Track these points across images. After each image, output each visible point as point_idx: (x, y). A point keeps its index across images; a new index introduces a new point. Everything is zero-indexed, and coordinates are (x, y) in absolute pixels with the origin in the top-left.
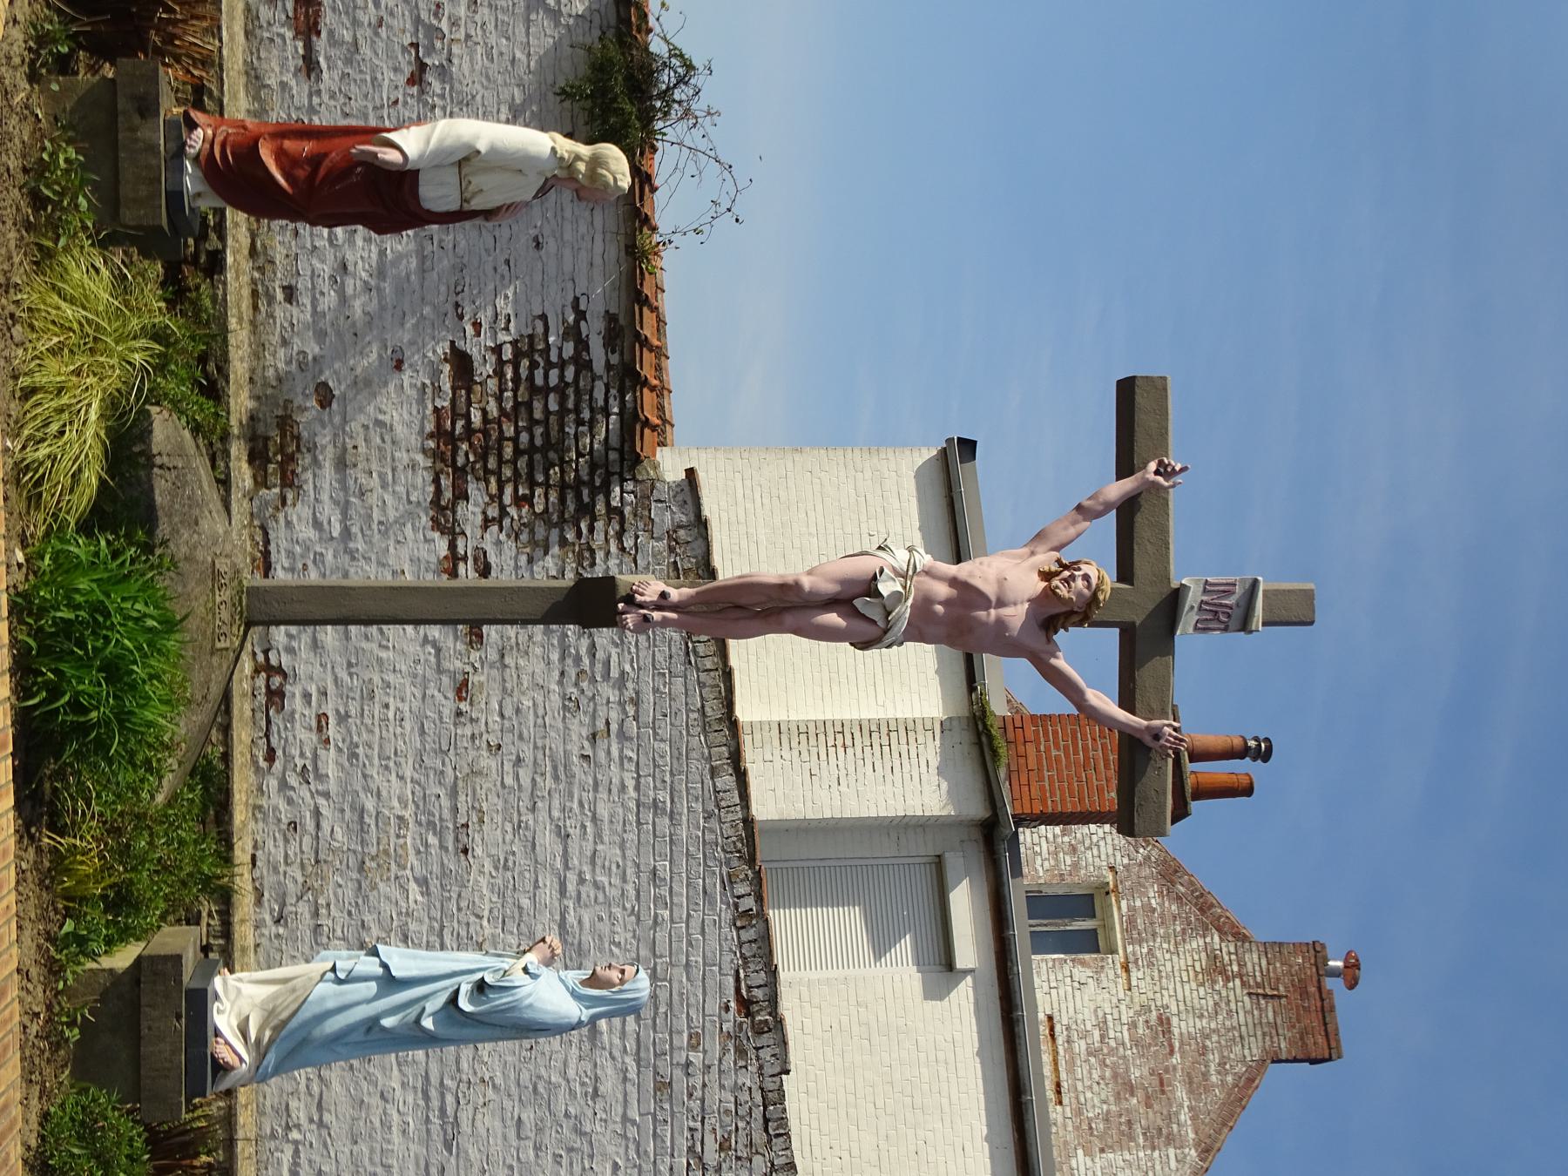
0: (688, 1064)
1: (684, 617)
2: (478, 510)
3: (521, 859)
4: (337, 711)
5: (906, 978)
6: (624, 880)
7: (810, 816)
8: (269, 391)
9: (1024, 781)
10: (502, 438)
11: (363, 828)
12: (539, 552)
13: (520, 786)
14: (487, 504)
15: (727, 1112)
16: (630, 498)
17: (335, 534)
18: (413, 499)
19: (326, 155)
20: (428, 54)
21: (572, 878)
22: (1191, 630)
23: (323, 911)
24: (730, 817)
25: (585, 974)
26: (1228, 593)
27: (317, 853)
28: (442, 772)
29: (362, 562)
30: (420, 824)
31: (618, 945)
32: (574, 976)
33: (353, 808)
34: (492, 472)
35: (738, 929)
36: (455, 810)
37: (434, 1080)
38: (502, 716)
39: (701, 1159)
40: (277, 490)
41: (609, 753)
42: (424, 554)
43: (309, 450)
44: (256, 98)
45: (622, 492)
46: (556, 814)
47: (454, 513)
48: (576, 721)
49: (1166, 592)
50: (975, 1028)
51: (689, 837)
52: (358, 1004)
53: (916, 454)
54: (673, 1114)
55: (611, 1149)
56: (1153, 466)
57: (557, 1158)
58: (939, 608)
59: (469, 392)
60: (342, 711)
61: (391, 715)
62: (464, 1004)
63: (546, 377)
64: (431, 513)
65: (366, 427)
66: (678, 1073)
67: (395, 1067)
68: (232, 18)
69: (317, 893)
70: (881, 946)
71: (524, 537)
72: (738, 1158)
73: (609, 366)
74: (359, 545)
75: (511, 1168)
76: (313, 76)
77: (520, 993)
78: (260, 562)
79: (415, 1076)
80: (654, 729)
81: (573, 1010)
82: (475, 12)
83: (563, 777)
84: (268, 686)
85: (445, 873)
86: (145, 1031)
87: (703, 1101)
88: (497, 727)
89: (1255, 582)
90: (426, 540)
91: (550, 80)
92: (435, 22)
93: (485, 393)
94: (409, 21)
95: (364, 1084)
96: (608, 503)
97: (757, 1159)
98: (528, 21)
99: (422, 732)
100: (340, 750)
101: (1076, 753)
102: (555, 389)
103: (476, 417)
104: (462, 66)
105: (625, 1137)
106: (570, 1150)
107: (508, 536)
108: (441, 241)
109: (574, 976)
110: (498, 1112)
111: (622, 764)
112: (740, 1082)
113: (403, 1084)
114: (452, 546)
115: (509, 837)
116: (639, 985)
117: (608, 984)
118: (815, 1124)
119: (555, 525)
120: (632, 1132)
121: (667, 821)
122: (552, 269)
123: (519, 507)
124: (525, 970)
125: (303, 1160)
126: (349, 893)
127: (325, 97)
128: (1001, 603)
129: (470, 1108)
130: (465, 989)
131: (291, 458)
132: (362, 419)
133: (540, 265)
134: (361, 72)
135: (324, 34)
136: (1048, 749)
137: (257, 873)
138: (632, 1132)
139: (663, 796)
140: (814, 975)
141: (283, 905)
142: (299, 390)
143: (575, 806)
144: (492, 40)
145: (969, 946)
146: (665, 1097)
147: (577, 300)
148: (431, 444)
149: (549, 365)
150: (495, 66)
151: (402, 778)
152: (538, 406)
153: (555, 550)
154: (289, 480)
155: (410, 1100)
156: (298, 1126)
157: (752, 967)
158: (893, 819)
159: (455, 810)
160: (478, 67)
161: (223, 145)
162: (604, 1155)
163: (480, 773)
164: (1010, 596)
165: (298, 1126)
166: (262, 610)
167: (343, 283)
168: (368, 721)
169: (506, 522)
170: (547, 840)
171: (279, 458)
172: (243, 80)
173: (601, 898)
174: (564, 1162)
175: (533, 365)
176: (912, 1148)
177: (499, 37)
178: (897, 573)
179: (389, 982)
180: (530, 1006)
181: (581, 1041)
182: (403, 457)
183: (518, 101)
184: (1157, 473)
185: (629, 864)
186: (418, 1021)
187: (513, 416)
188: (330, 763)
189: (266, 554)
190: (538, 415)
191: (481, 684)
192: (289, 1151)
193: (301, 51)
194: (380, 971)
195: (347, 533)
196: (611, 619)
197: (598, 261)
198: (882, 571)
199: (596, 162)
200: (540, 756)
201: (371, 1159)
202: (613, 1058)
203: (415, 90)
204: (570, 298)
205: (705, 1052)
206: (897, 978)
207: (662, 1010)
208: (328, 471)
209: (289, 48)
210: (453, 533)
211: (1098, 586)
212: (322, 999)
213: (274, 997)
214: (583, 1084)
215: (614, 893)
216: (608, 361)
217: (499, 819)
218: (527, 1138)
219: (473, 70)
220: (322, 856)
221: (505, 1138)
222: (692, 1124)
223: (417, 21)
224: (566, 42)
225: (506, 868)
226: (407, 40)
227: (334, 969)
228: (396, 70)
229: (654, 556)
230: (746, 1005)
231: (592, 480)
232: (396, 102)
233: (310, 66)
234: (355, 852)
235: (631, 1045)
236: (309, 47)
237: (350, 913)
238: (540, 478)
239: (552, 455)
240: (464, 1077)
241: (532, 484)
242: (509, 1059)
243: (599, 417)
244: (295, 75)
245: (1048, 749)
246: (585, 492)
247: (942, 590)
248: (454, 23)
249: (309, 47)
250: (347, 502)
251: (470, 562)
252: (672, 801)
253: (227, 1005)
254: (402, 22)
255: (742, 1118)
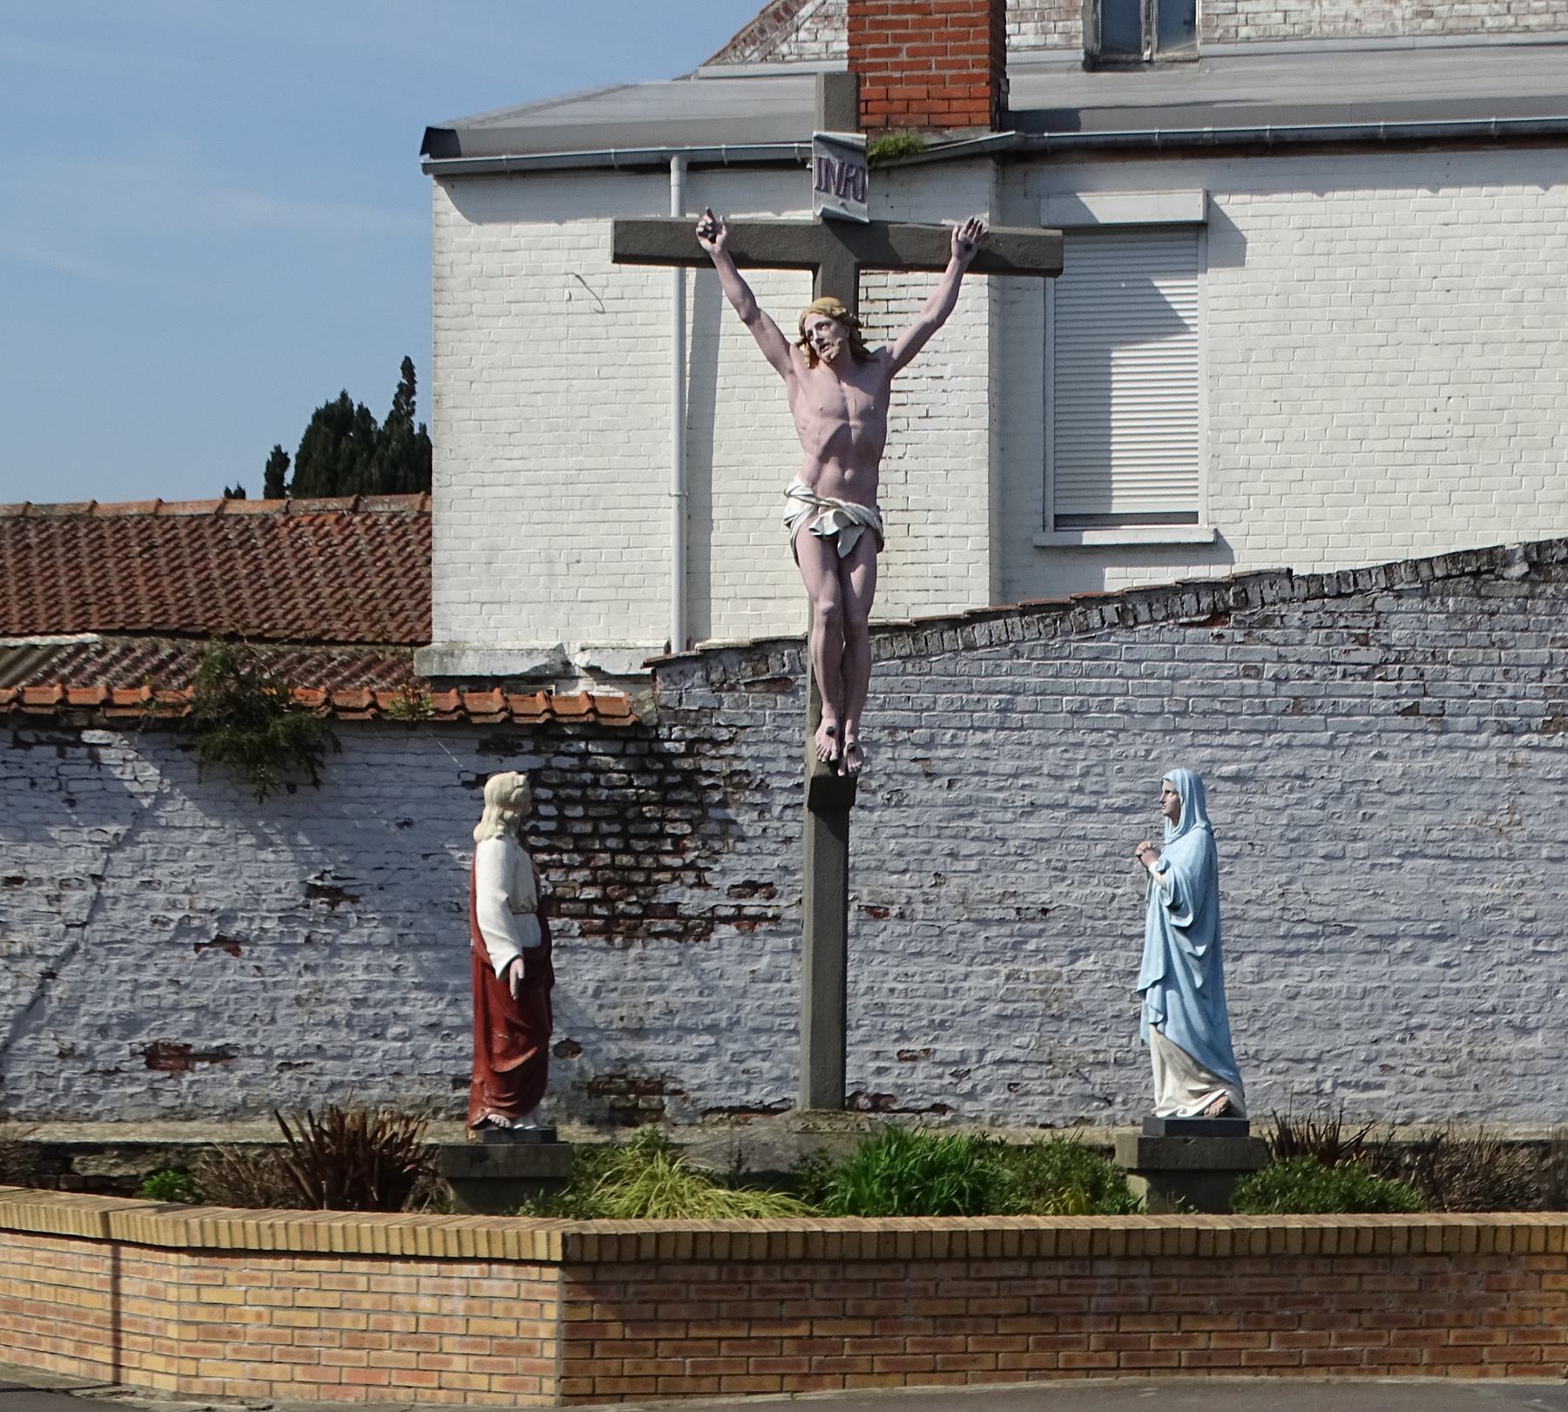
0: (1276, 678)
1: (850, 713)
2: (688, 893)
3: (1055, 854)
4: (896, 1040)
5: (1212, 290)
6: (1081, 744)
7: (985, 421)
8: (563, 1105)
9: (943, 106)
10: (612, 866)
11: (1018, 1016)
12: (733, 829)
13: (979, 854)
14: (682, 883)
15: (1328, 637)
16: (676, 732)
17: (712, 1040)
18: (676, 960)
19: (507, 1020)
20: (206, 933)
21: (1076, 800)
22: (865, 206)
23: (1101, 1057)
24: (1018, 630)
25: (1167, 821)
26: (829, 165)
27: (1041, 1063)
28: (962, 934)
29: (742, 1013)
30: (1015, 957)
31: (1148, 752)
32: (1169, 831)
33: (997, 1026)
34: (648, 877)
35: (1137, 623)
36: (1002, 921)
37: (1279, 944)
38: (905, 871)
39: (1375, 666)
40: (666, 1099)
41: (946, 759)
42: (735, 950)
43: (624, 1066)
44: (256, 1111)
45: (669, 740)
46: (1009, 816)
47: (691, 918)
48: (912, 793)
49: (827, 230)
50: (1286, 196)
51: (1038, 675)
52: (1183, 1005)
53: (444, 219)
54: (1326, 696)
55: (1360, 762)
56: (705, 243)
57: (1367, 818)
58: (848, 474)
59: (563, 899)
60: (896, 1036)
61: (901, 986)
62: (1187, 922)
63: (547, 818)
64: (691, 941)
65: (601, 1007)
66: (1285, 689)
67: (1263, 985)
68: (176, 1133)
69: (1082, 1063)
70: (1165, 323)
71: (717, 845)
72: (1377, 626)
73: (536, 752)
74: (723, 1017)
75: (1373, 866)
76: (232, 1053)
77: (1180, 876)
78: (740, 1117)
79: (1273, 965)
80: (922, 711)
81: (1197, 833)
82: (160, 883)
83: (970, 809)
84: (868, 1111)
85: (1066, 933)
86: (1196, 1166)
87: (1315, 664)
88: (916, 877)
89: (818, 138)
90: (720, 947)
91: (228, 806)
92: (172, 926)
93: (565, 884)
94: (172, 953)
95: (1279, 1016)
96: (682, 756)
97: (1379, 605)
98: (168, 827)
99: (920, 954)
100: (936, 1039)
101: (904, 24)
102: (560, 809)
103: (590, 893)
104: (220, 899)
105: (1348, 746)
106: (1358, 804)
107: (716, 861)
108: (404, 926)
109: (1169, 831)
110: (1316, 879)
111: (958, 746)
112: (1298, 623)
113: (1282, 977)
114: (726, 920)
115: (1031, 866)
116: (1179, 778)
117: (1177, 806)
118: (1404, 431)
119: (705, 812)
120: (1344, 739)
121: (1020, 698)
122: (433, 810)
123: (685, 850)
124: (1162, 872)
125: (1353, 1078)
126: (1084, 1030)
127: (254, 1041)
128: (844, 415)
129: (1310, 908)
130: (1175, 921)
131: (633, 1085)
132: (592, 1011)
133: (429, 823)
134: (227, 1003)
135: (188, 1041)
136: (900, 66)
137: (1060, 1123)
138: (1344, 739)
139: (994, 701)
140: (1204, 421)
141: (1093, 1097)
142: (562, 1074)
143: (1001, 795)
144: (190, 866)
145: (1175, 200)
146: (1309, 703)
147: (465, 784)
148: (618, 940)
149: (535, 815)
150: (218, 864)
151: (966, 976)
152: (578, 828)
153: (731, 812)
154: (656, 1086)
155: (1298, 970)
156: (1319, 1083)
157: (1177, 608)
158: (992, 300)
159: (1002, 921)
160: (219, 882)
161: (500, 1100)
162: (1365, 768)
163: (964, 895)
164: (837, 405)
165: (1319, 1083)
166: (832, 1092)
167: (449, 1028)
168: (907, 1010)
169: (701, 863)
170: (1036, 826)
171: (632, 1096)
172: (238, 1124)
173: (1099, 770)
174: (1370, 811)
175: (535, 831)
176: (1441, 296)
177: (186, 860)
178: (814, 514)
179: (1167, 981)
180: (1191, 869)
181: (1247, 792)
182: (631, 970)
183: (254, 841)
184: (713, 240)
185: (1064, 739)
186: (1199, 959)
187: (588, 853)
188: (949, 1048)
189: (732, 1110)
190: (588, 828)
191: (871, 893)
192: (1342, 1092)
193: (206, 1065)
194: (1158, 987)
195: (712, 1029)
196: (850, 783)
197: (423, 760)
198: (813, 530)
199: (504, 802)
200: (948, 832)
201: (1356, 1010)
202: (1266, 758)
203: (245, 949)
204: (463, 791)
205: (1264, 661)
206: (1213, 303)
207: (1218, 706)
208: (647, 1047)
209: (203, 1076)
210: (711, 920)
211: (830, 315)
212: (1178, 1032)
213: (1175, 1070)
214: (1291, 790)
215: (1094, 755)
216: (530, 753)
217: (1012, 876)
218: (1344, 849)
219: (222, 887)
220: (1045, 1058)
221: (1342, 872)
222: (1338, 676)
223: (171, 943)
224: (194, 787)
225: (1063, 869)
226: (192, 955)
227: (1155, 1024)
228: (224, 967)
229: (738, 707)
230: (1217, 616)
231: (657, 772)
232: (258, 968)
233: (221, 1056)
234: (1041, 1025)
235: (1253, 740)
236: (201, 1057)
237: (1104, 1030)
238: (655, 827)
239: (631, 813)
240: (1278, 914)
241: (661, 835)
242: (1261, 867)
243: (590, 762)
244: (231, 1072)
245: (900, 66)
246: (670, 779)
247: (831, 470)
248: (173, 905)
249: (201, 1057)
250: (679, 1028)
251: (743, 902)
252: (999, 692)
253: (1180, 1107)
254: (173, 959)
255: (1335, 621)
